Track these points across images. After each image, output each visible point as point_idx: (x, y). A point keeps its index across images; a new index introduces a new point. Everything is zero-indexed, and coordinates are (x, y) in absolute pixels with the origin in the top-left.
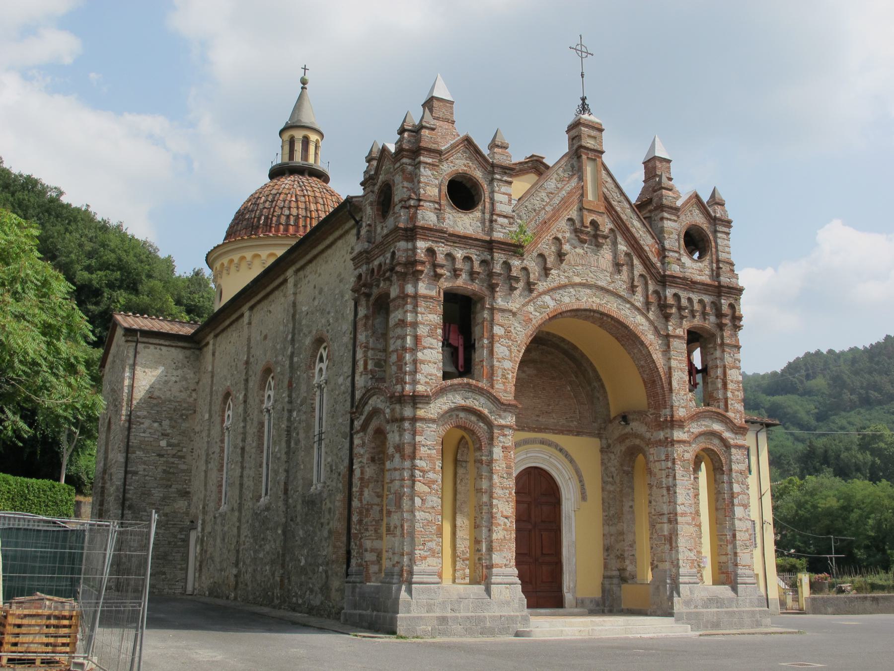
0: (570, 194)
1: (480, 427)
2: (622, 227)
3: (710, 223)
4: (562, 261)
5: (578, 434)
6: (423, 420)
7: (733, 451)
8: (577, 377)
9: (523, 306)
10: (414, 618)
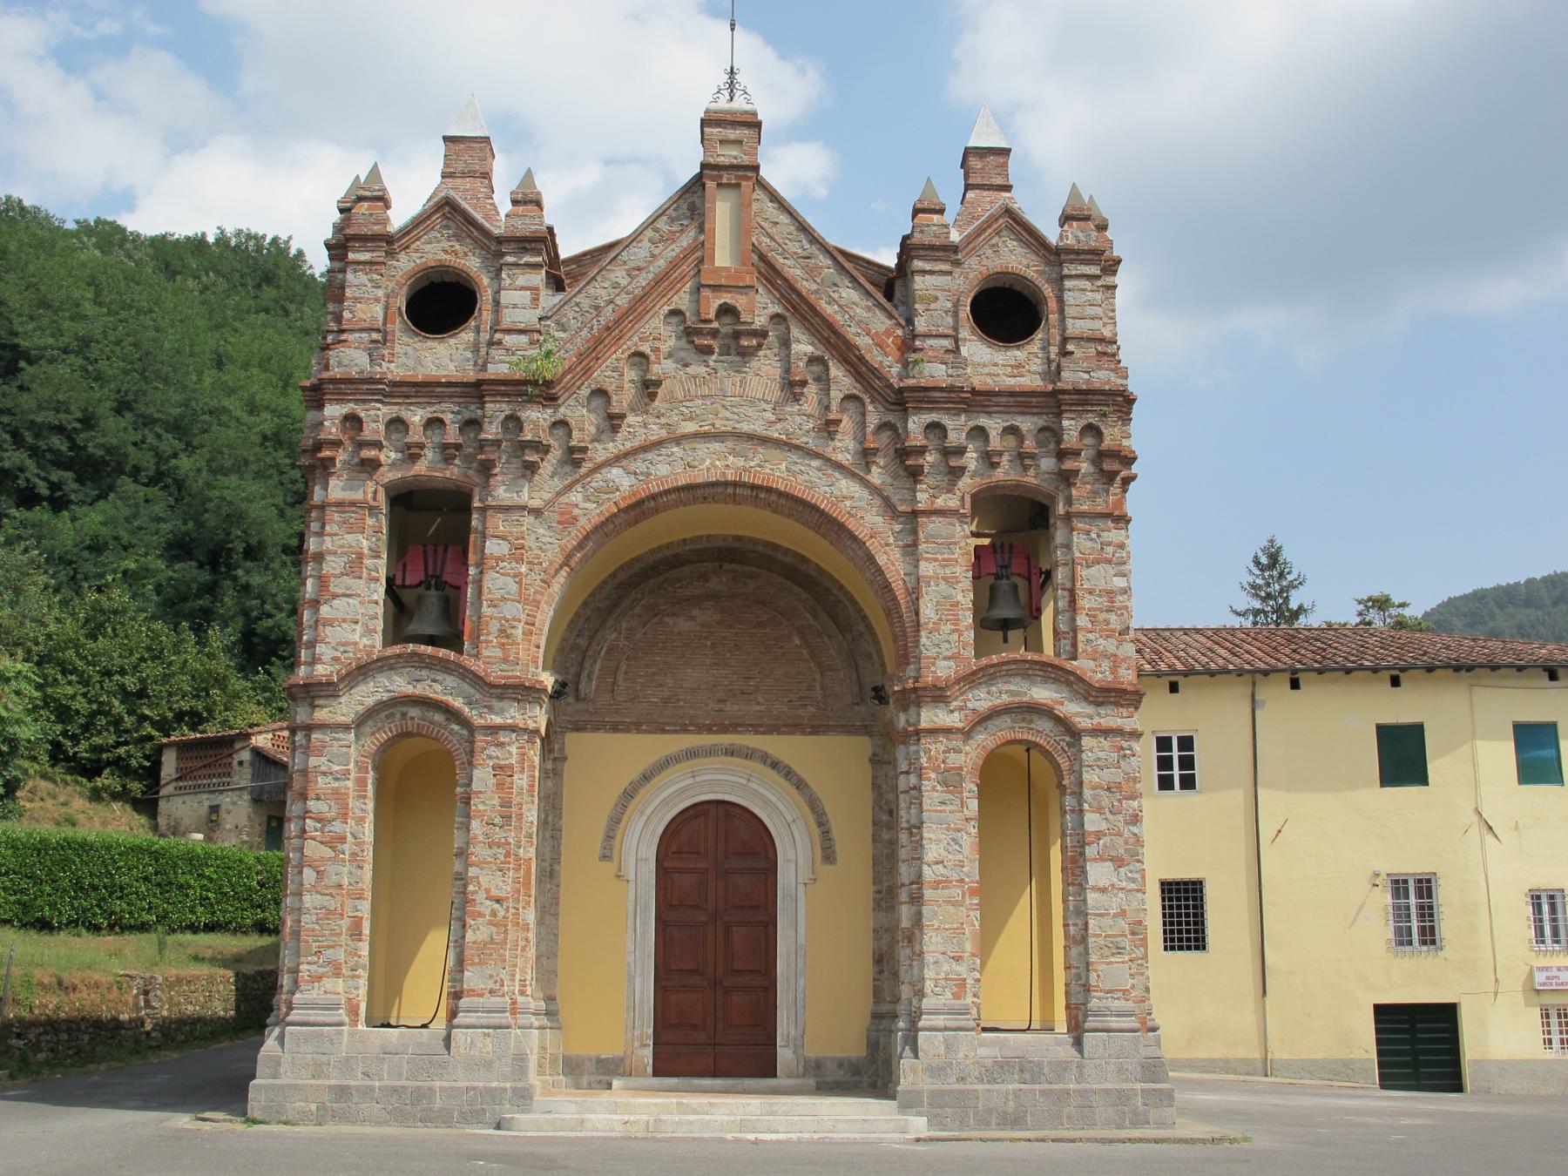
0: (675, 264)
1: (452, 732)
2: (799, 308)
3: (1048, 263)
4: (653, 397)
5: (816, 730)
6: (323, 727)
7: (1086, 741)
8: (816, 617)
9: (559, 494)
10: (282, 1086)
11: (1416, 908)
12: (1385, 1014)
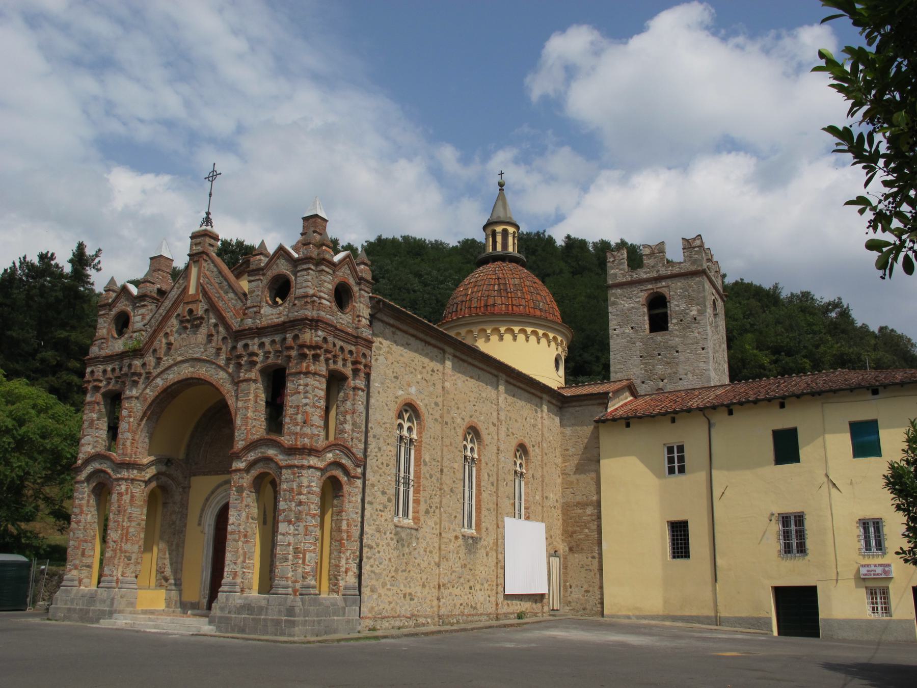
7: (284, 471)
11: (793, 533)
12: (779, 592)
